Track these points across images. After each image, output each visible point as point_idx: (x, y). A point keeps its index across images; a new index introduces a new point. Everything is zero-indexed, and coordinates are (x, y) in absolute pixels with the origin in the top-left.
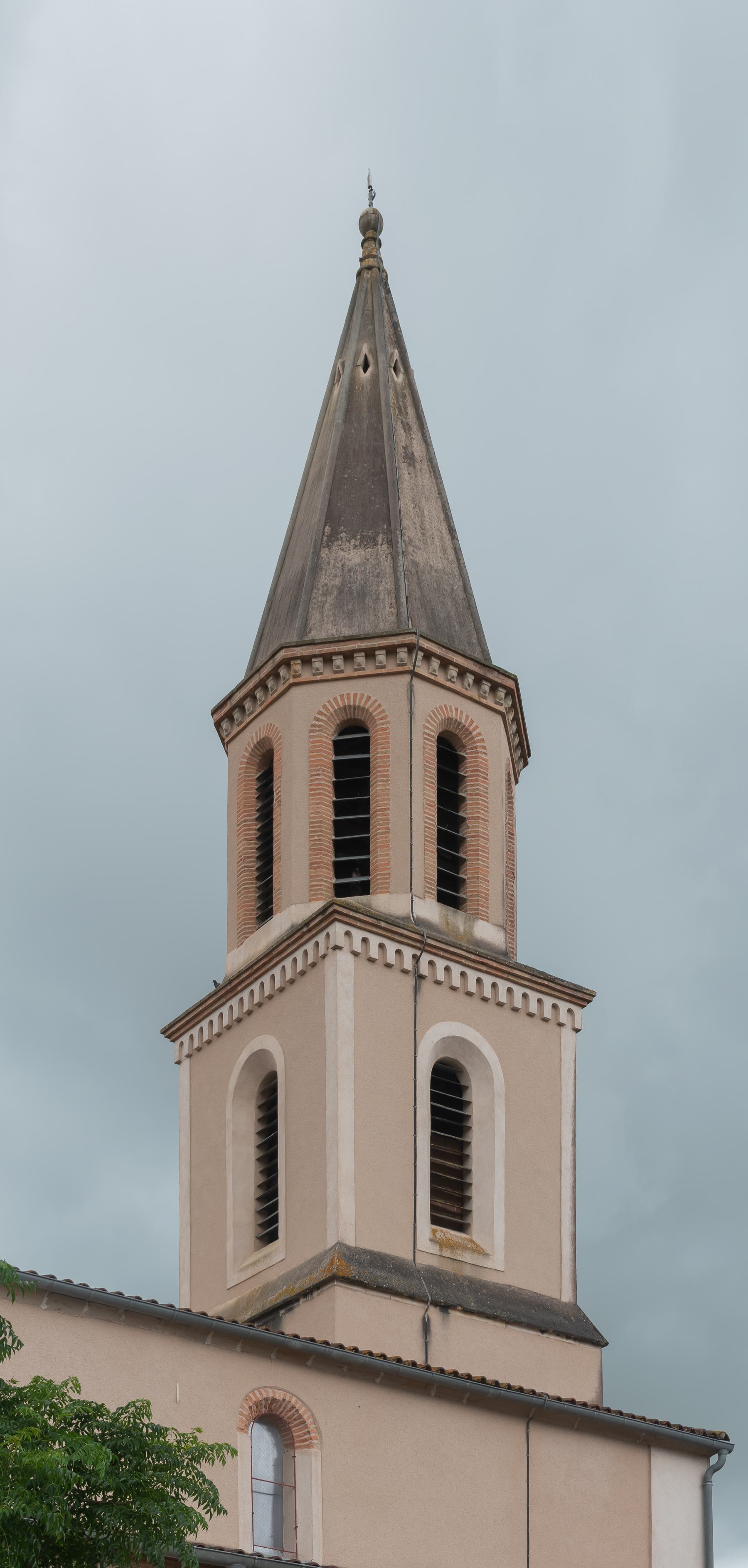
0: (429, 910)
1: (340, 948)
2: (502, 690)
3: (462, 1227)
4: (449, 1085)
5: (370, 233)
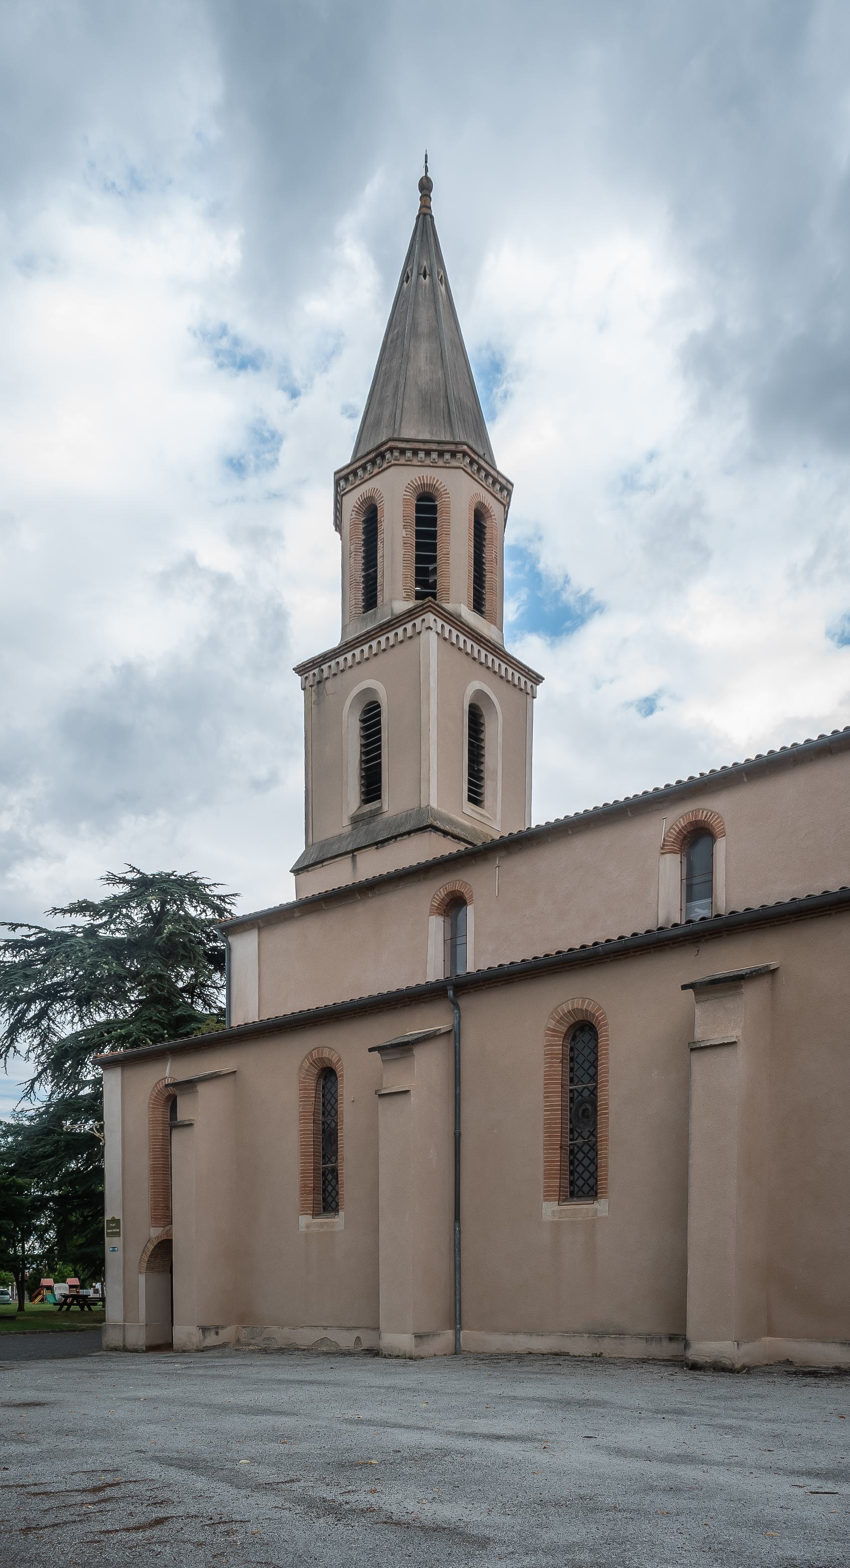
1: (431, 629)
2: (502, 488)
5: (425, 192)
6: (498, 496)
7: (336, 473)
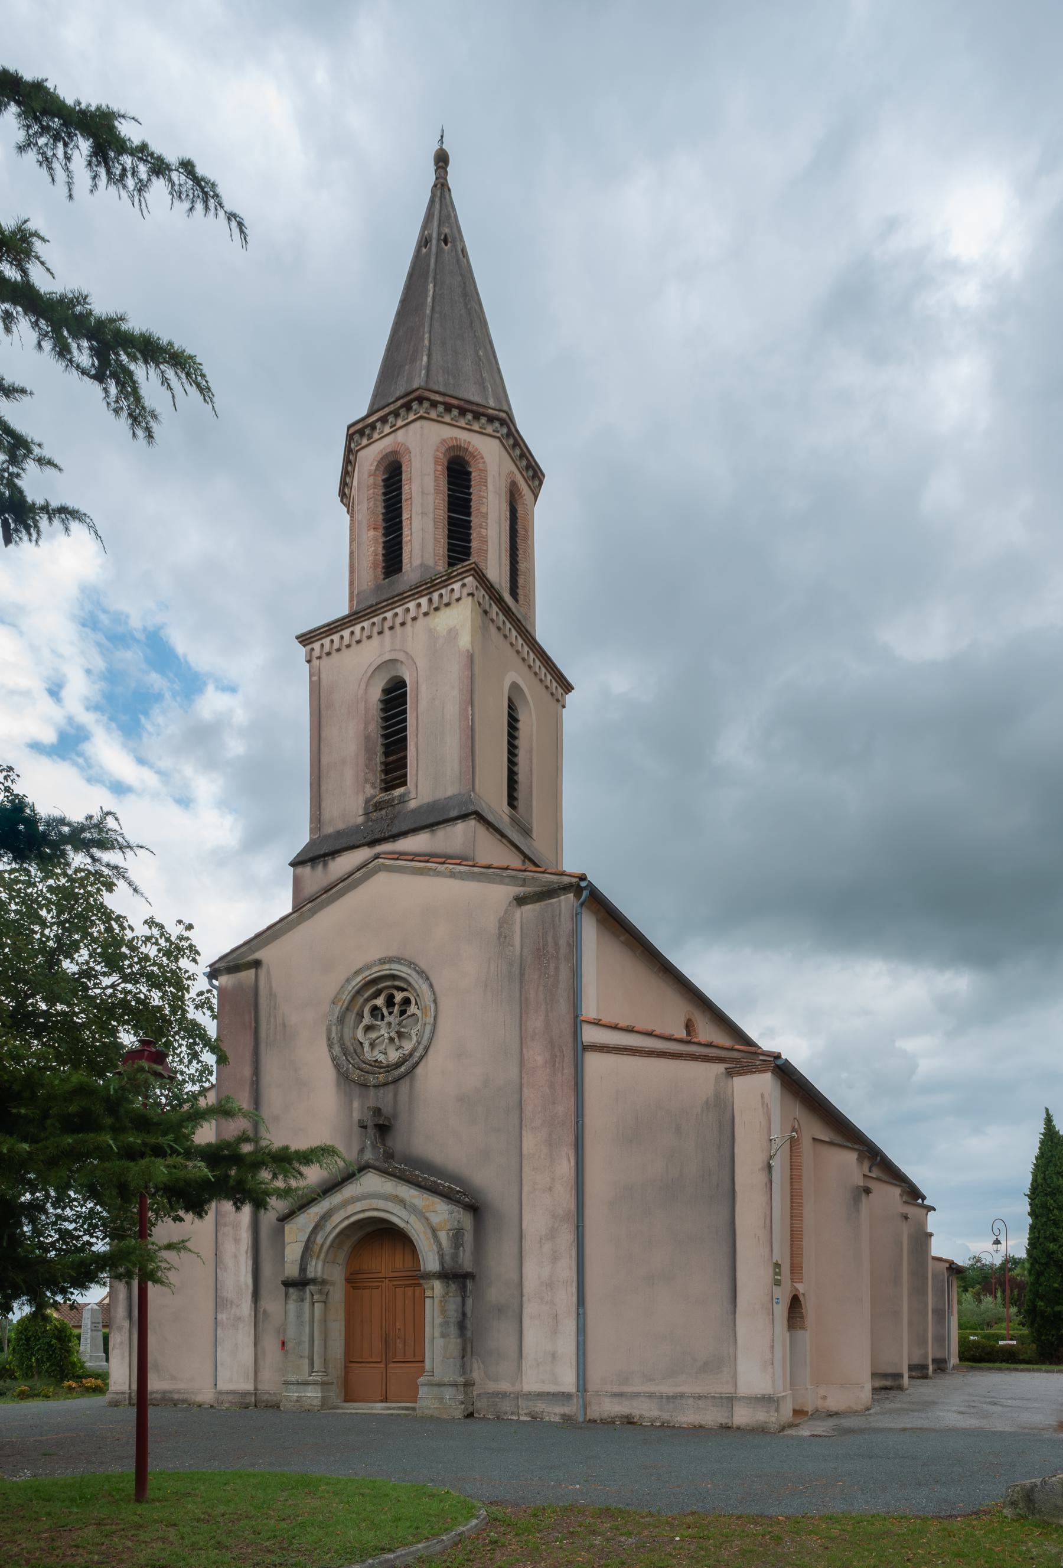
6: (530, 483)
7: (349, 427)
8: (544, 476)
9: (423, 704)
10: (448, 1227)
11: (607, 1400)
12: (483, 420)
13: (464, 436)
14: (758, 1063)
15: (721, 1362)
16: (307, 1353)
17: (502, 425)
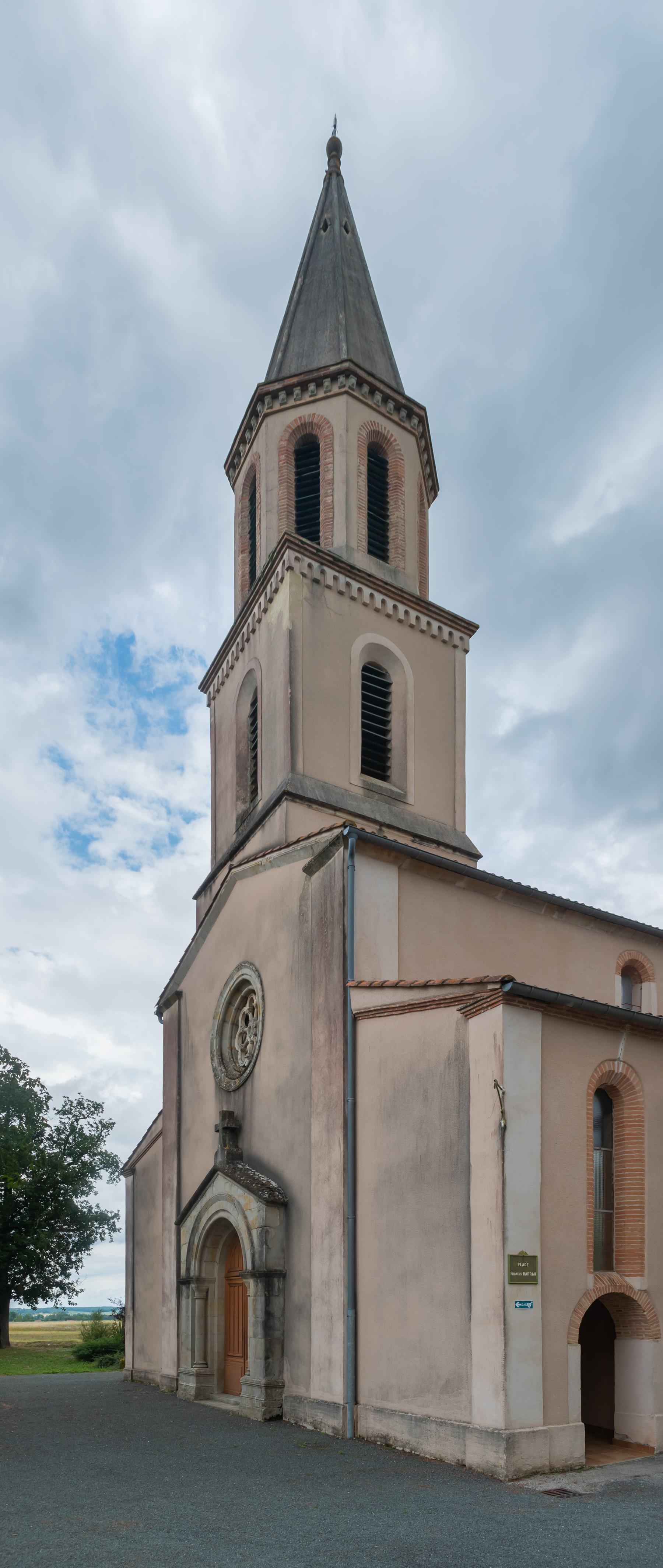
0: (363, 561)
2: (412, 414)
3: (385, 778)
4: (376, 686)
6: (407, 425)
8: (423, 409)
9: (265, 701)
10: (257, 1225)
11: (371, 1416)
12: (327, 382)
13: (304, 412)
14: (485, 995)
15: (456, 1384)
16: (190, 1347)
17: (347, 377)
